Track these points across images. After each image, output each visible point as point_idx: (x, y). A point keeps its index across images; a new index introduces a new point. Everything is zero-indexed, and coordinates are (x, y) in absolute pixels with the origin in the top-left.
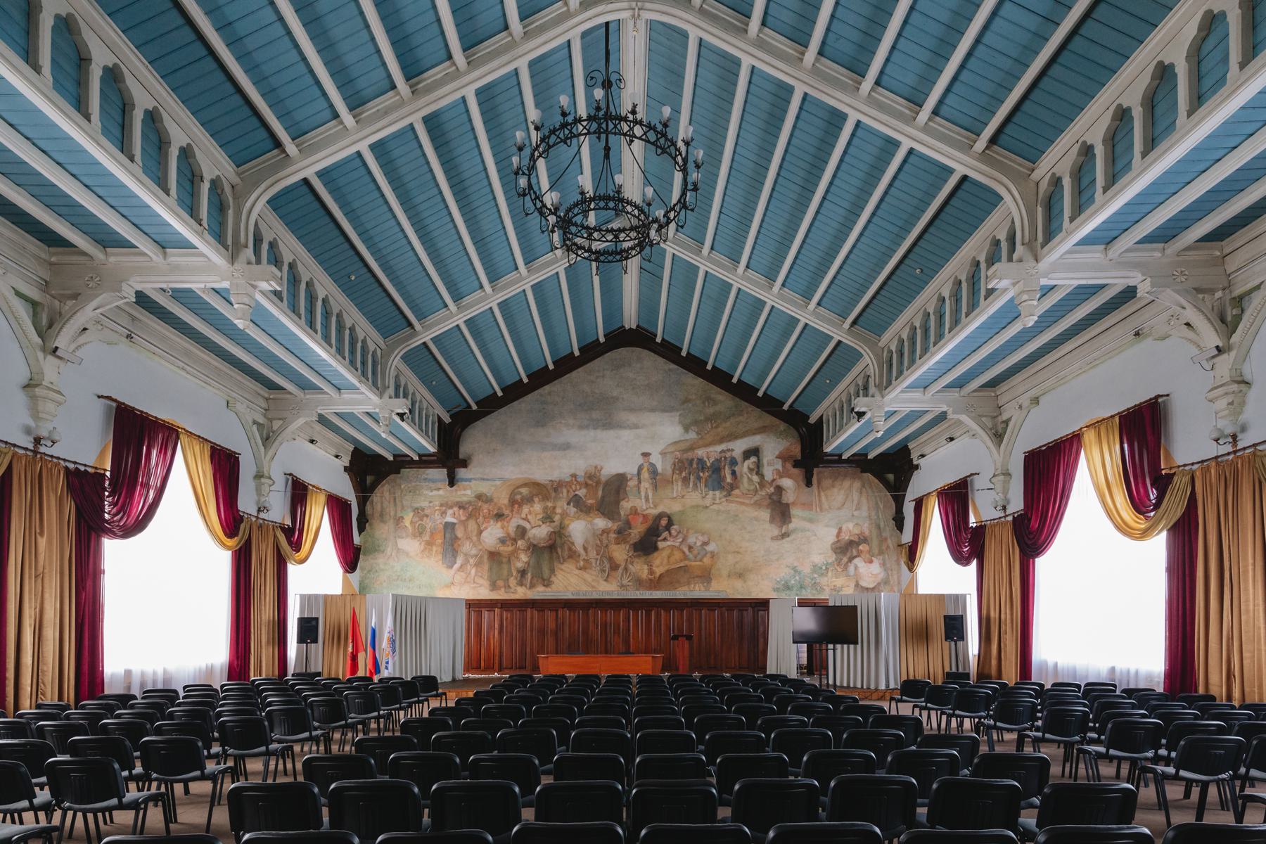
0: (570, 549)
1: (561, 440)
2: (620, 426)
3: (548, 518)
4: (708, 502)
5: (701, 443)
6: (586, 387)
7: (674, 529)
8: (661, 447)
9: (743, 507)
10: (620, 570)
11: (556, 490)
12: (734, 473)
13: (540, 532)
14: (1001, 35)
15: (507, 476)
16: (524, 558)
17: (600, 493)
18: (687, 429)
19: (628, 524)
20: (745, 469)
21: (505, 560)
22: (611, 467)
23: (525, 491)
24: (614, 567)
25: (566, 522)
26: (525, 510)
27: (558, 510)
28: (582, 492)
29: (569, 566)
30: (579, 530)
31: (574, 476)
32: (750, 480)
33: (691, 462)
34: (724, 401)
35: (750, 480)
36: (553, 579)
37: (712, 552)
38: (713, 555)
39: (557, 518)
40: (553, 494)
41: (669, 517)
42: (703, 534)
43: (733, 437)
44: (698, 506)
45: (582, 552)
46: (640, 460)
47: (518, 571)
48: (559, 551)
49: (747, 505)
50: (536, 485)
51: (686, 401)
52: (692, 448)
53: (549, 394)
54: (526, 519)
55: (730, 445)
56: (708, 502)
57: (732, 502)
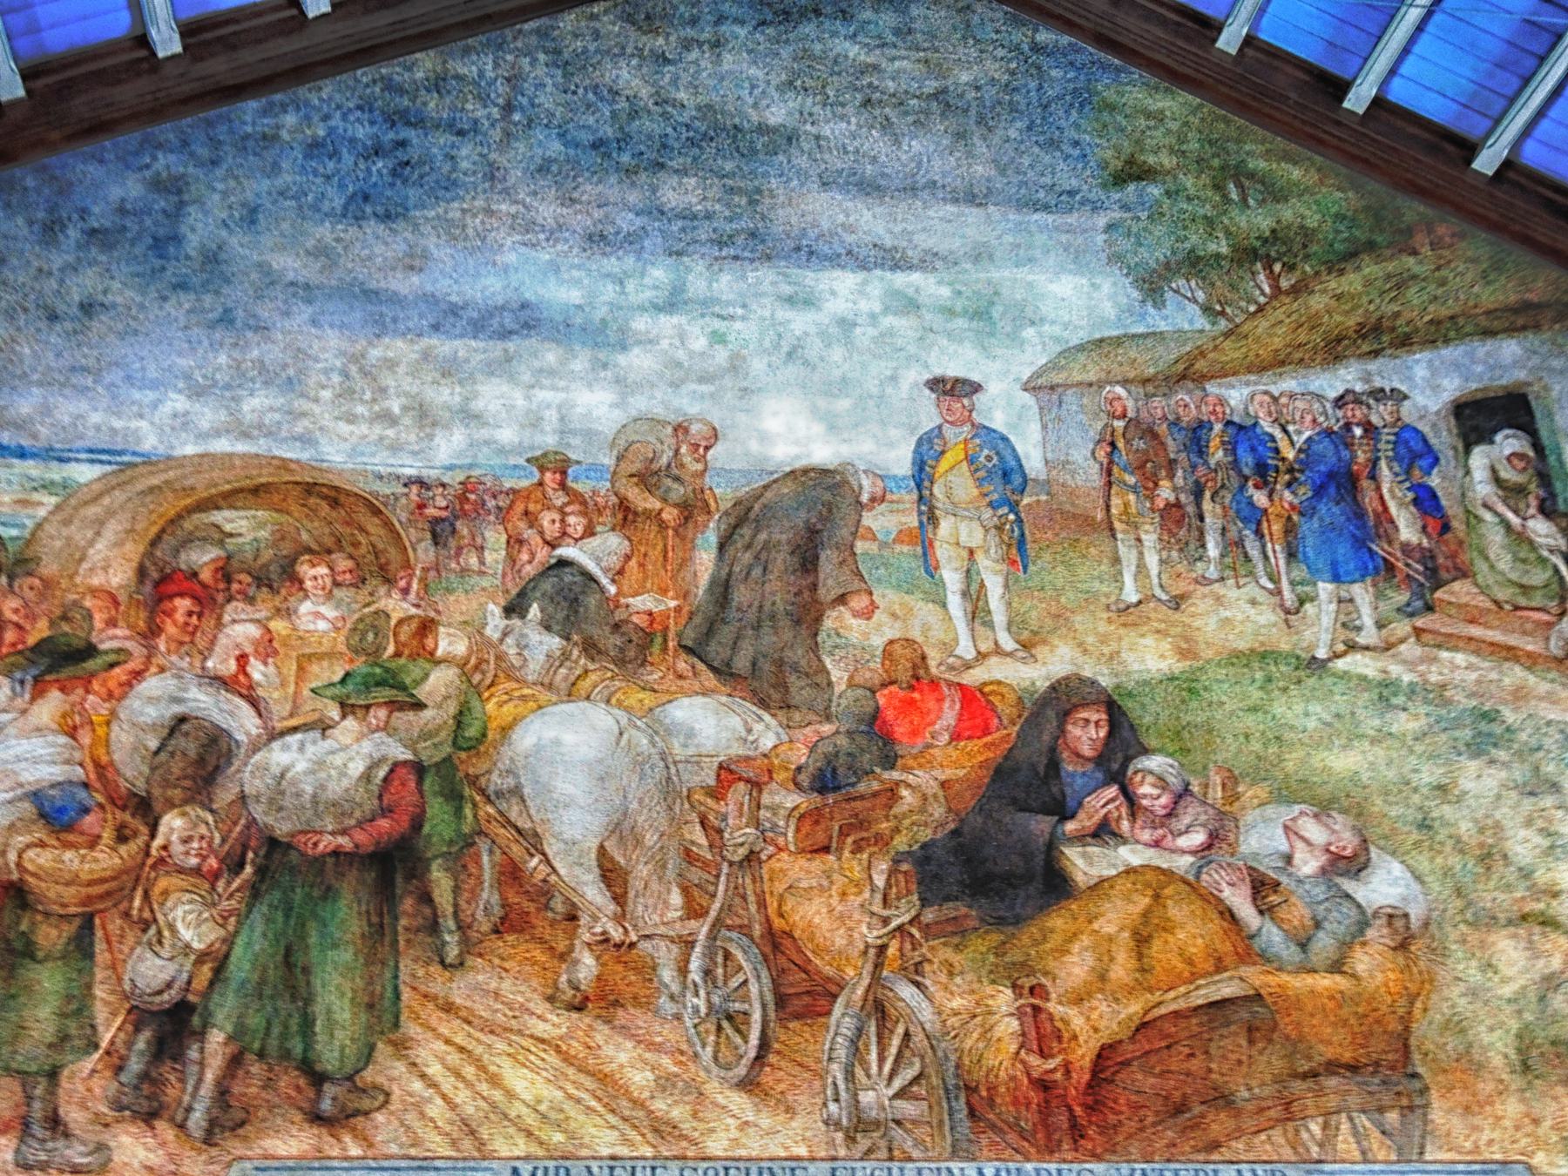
0: (511, 873)
1: (487, 287)
2: (809, 251)
3: (379, 685)
4: (1319, 628)
5: (1232, 352)
6: (627, 77)
7: (1155, 768)
8: (1032, 357)
9: (1516, 674)
10: (842, 1018)
11: (440, 531)
12: (1426, 501)
13: (323, 766)
14: (1546, 145)
15: (150, 442)
16: (190, 923)
17: (705, 560)
18: (1152, 286)
19: (878, 737)
20: (1482, 488)
21: (50, 936)
22: (781, 433)
23: (245, 526)
24: (802, 995)
25: (494, 709)
26: (240, 628)
27: (450, 643)
28: (595, 553)
29: (500, 984)
30: (572, 758)
31: (556, 465)
32: (1518, 538)
33: (1196, 437)
34: (1313, 196)
35: (1518, 538)
36: (388, 1070)
37: (1394, 917)
38: (1404, 935)
39: (438, 683)
40: (424, 553)
41: (1113, 709)
42: (1323, 809)
43: (1380, 336)
44: (1265, 655)
45: (593, 893)
46: (928, 413)
47: (139, 1016)
48: (440, 880)
49: (1531, 661)
50: (322, 493)
51: (1132, 172)
52: (1188, 374)
53: (438, 84)
54: (237, 684)
55: (1385, 372)
56: (1319, 628)
57: (1450, 642)
